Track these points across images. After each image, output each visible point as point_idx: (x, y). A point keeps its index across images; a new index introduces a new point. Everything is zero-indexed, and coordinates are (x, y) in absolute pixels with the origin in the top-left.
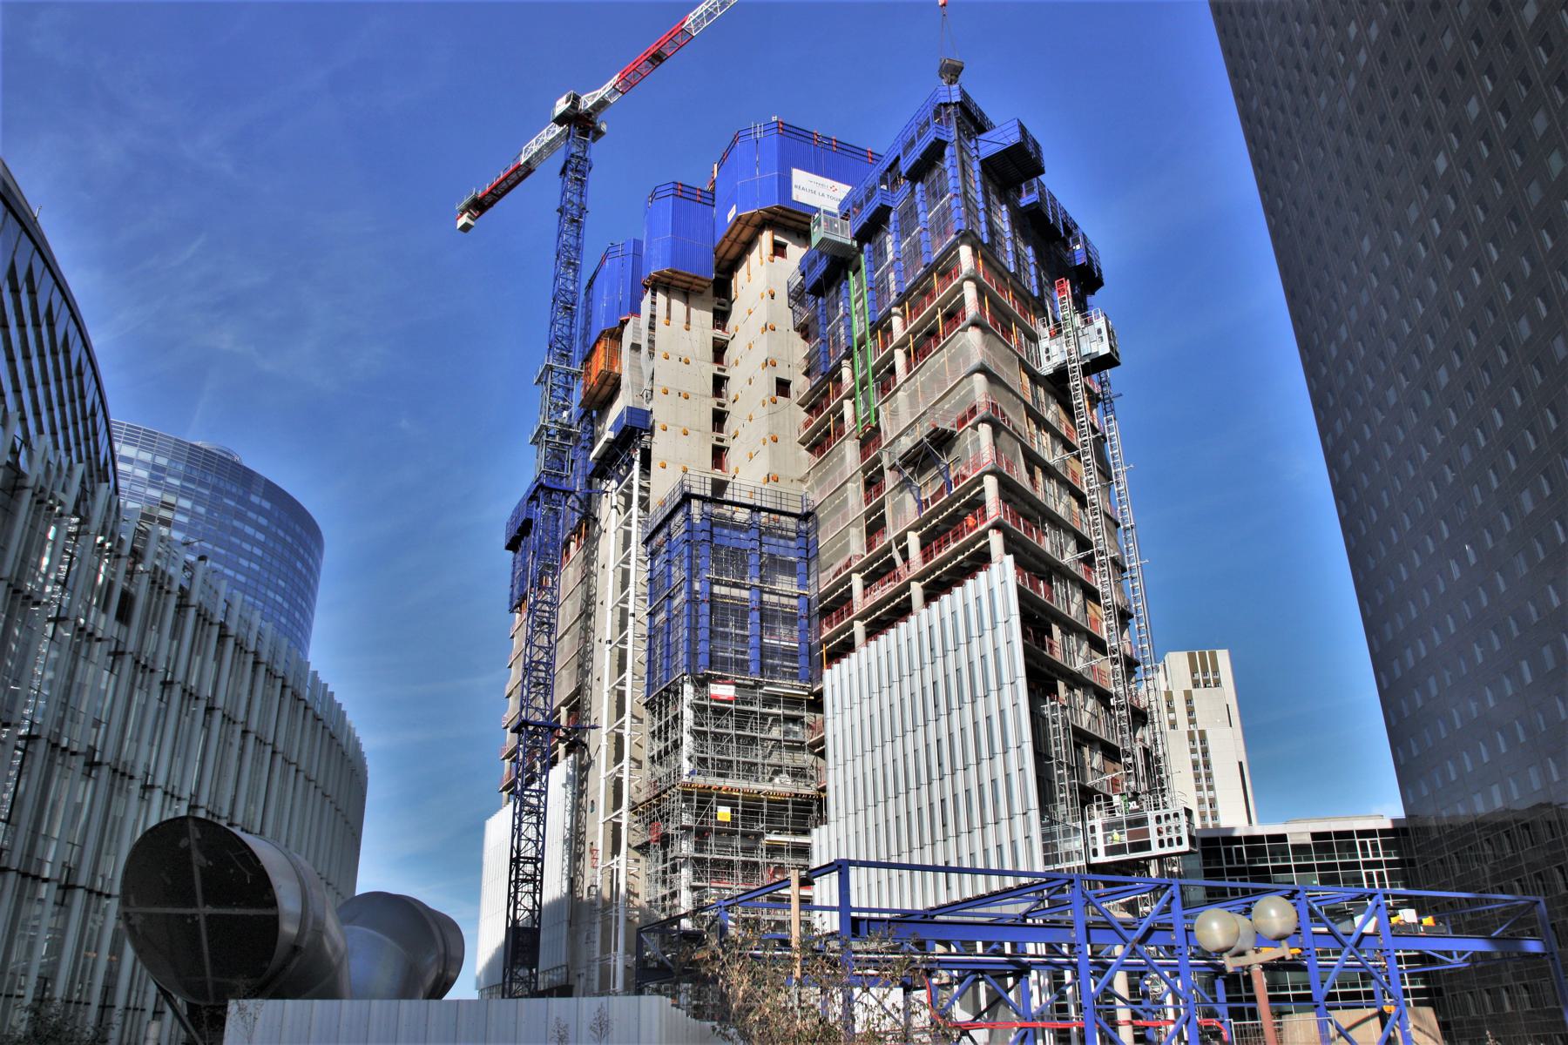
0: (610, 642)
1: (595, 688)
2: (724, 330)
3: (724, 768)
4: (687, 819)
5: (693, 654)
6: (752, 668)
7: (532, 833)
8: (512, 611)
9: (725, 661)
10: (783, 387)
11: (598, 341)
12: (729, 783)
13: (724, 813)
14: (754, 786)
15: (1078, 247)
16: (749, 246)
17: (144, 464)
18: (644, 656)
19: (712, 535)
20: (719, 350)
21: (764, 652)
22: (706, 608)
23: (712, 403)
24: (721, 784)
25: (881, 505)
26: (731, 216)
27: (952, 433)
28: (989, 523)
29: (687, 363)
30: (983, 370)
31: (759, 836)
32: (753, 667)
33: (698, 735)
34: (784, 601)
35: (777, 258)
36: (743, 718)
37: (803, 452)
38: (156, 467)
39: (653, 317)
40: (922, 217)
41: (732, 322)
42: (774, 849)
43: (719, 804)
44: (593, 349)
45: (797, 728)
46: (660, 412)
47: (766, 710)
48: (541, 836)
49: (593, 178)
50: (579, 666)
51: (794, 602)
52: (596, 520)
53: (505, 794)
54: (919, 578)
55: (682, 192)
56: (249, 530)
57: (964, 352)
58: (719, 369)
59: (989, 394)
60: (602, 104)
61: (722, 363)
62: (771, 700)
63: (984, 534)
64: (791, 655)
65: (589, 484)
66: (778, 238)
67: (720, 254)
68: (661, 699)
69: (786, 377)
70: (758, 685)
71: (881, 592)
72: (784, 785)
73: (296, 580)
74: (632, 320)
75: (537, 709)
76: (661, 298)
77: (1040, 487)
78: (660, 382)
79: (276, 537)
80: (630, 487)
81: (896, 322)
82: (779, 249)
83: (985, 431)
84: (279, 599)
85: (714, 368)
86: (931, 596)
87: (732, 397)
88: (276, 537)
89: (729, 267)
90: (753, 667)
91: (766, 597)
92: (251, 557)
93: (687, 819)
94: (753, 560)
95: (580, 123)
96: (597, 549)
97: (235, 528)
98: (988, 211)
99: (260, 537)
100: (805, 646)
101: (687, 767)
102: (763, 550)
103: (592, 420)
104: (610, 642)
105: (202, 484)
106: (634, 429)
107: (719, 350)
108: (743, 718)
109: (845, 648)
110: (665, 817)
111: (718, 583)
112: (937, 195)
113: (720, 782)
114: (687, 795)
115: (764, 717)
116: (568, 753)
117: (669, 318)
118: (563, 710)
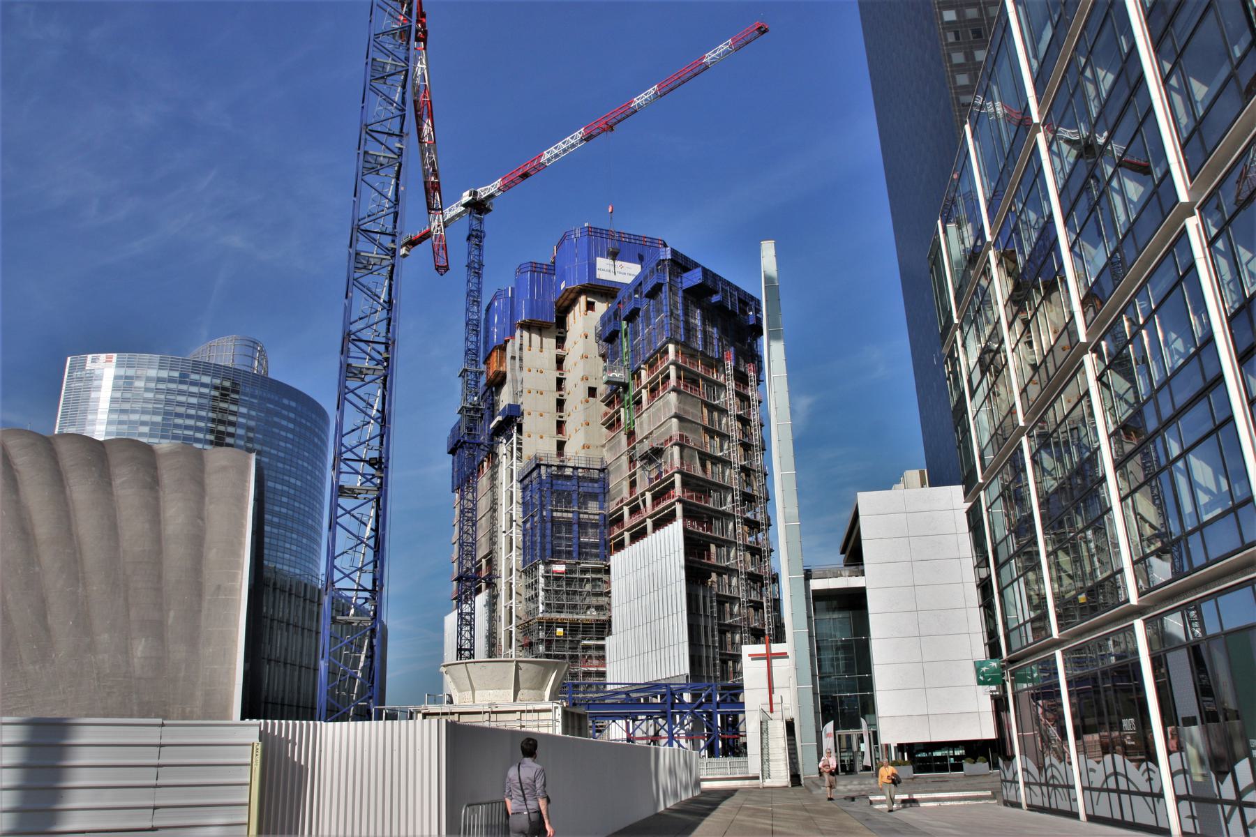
0: (504, 532)
1: (499, 553)
2: (562, 349)
3: (560, 608)
4: (542, 635)
5: (543, 549)
6: (574, 555)
7: (468, 635)
8: (453, 492)
9: (560, 552)
10: (592, 392)
11: (493, 350)
12: (563, 616)
13: (560, 631)
14: (576, 617)
15: (751, 313)
16: (574, 302)
17: (216, 388)
18: (521, 538)
19: (552, 485)
20: (560, 361)
21: (581, 545)
22: (549, 525)
23: (556, 395)
24: (558, 617)
25: (634, 474)
26: (563, 286)
27: (662, 449)
28: (675, 499)
29: (542, 372)
30: (676, 416)
31: (579, 642)
32: (575, 555)
33: (546, 591)
34: (591, 517)
35: (589, 312)
36: (570, 582)
37: (604, 430)
38: (224, 389)
39: (521, 345)
40: (653, 320)
41: (568, 344)
42: (586, 648)
43: (557, 627)
44: (490, 354)
45: (600, 583)
46: (526, 404)
47: (583, 576)
48: (473, 637)
49: (486, 243)
50: (491, 539)
51: (597, 517)
52: (497, 455)
53: (455, 602)
54: (650, 517)
55: (535, 268)
56: (284, 423)
57: (667, 403)
58: (560, 374)
59: (680, 429)
60: (491, 196)
61: (562, 370)
62: (584, 571)
63: (673, 504)
64: (595, 545)
65: (492, 440)
66: (589, 299)
67: (559, 304)
68: (529, 571)
69: (594, 386)
70: (579, 563)
71: (637, 519)
72: (592, 615)
73: (315, 450)
74: (511, 341)
75: (468, 500)
76: (526, 334)
77: (709, 471)
78: (527, 386)
79: (300, 425)
80: (512, 444)
81: (644, 373)
82: (590, 306)
83: (676, 449)
84: (305, 464)
85: (557, 374)
86: (654, 530)
87: (567, 391)
88: (300, 425)
89: (563, 311)
90: (575, 555)
91: (581, 516)
92: (286, 440)
93: (542, 635)
94: (575, 496)
95: (478, 207)
96: (497, 472)
97: (275, 422)
98: (686, 314)
99: (291, 426)
100: (603, 541)
101: (541, 608)
102: (580, 490)
103: (492, 392)
104: (504, 532)
105: (253, 396)
106: (512, 417)
107: (560, 361)
108: (570, 582)
109: (620, 546)
110: (531, 633)
111: (557, 511)
112: (659, 311)
113: (557, 616)
114: (540, 623)
115: (581, 580)
116: (486, 588)
117: (530, 346)
118: (484, 560)
